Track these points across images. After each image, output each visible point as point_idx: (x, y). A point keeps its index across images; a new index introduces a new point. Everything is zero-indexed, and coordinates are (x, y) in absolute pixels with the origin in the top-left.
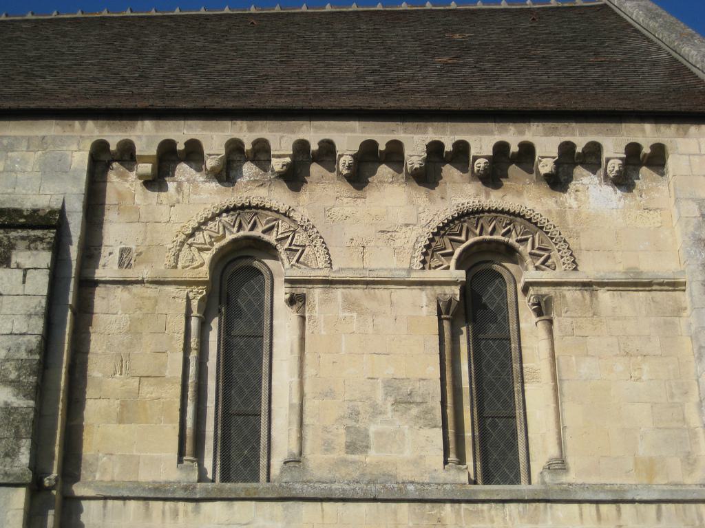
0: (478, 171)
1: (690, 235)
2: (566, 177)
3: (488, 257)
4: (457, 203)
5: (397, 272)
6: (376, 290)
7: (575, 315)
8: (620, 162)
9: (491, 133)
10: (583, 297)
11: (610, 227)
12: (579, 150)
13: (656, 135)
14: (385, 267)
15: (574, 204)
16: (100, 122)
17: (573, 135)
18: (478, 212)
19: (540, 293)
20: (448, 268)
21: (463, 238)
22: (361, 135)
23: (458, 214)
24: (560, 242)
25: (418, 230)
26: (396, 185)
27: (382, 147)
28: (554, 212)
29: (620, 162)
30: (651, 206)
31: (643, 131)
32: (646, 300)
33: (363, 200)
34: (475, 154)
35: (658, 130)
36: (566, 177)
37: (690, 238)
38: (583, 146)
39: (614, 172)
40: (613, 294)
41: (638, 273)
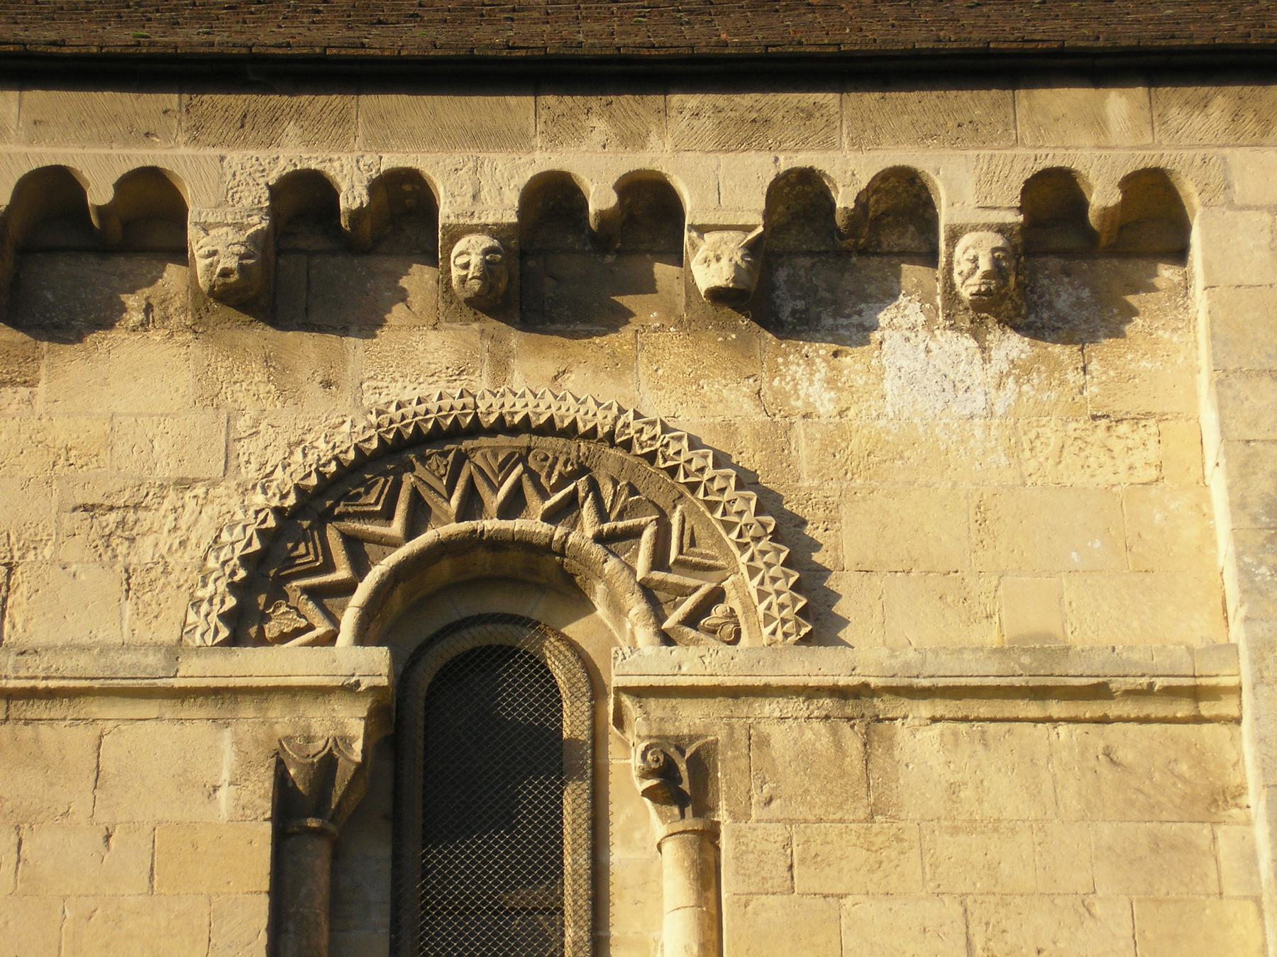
0: (463, 280)
1: (1259, 509)
2: (800, 304)
3: (500, 602)
4: (384, 400)
5: (129, 658)
6: (44, 729)
7: (802, 812)
8: (999, 241)
9: (516, 140)
10: (838, 745)
11: (955, 485)
12: (844, 200)
13: (1148, 139)
14: (85, 640)
15: (825, 403)
16: (1084, 188)
17: (827, 144)
18: (457, 432)
19: (670, 730)
20: (330, 639)
21: (396, 527)
22: (24, 149)
23: (381, 439)
24: (757, 539)
25: (226, 499)
26: (157, 336)
27: (100, 194)
28: (744, 430)
29: (999, 241)
30: (1120, 406)
31: (1098, 123)
32: (1083, 753)
33: (24, 391)
34: (453, 220)
35: (1156, 120)
36: (800, 304)
37: (1255, 519)
38: (864, 181)
39: (976, 278)
40: (955, 734)
41: (1050, 654)
